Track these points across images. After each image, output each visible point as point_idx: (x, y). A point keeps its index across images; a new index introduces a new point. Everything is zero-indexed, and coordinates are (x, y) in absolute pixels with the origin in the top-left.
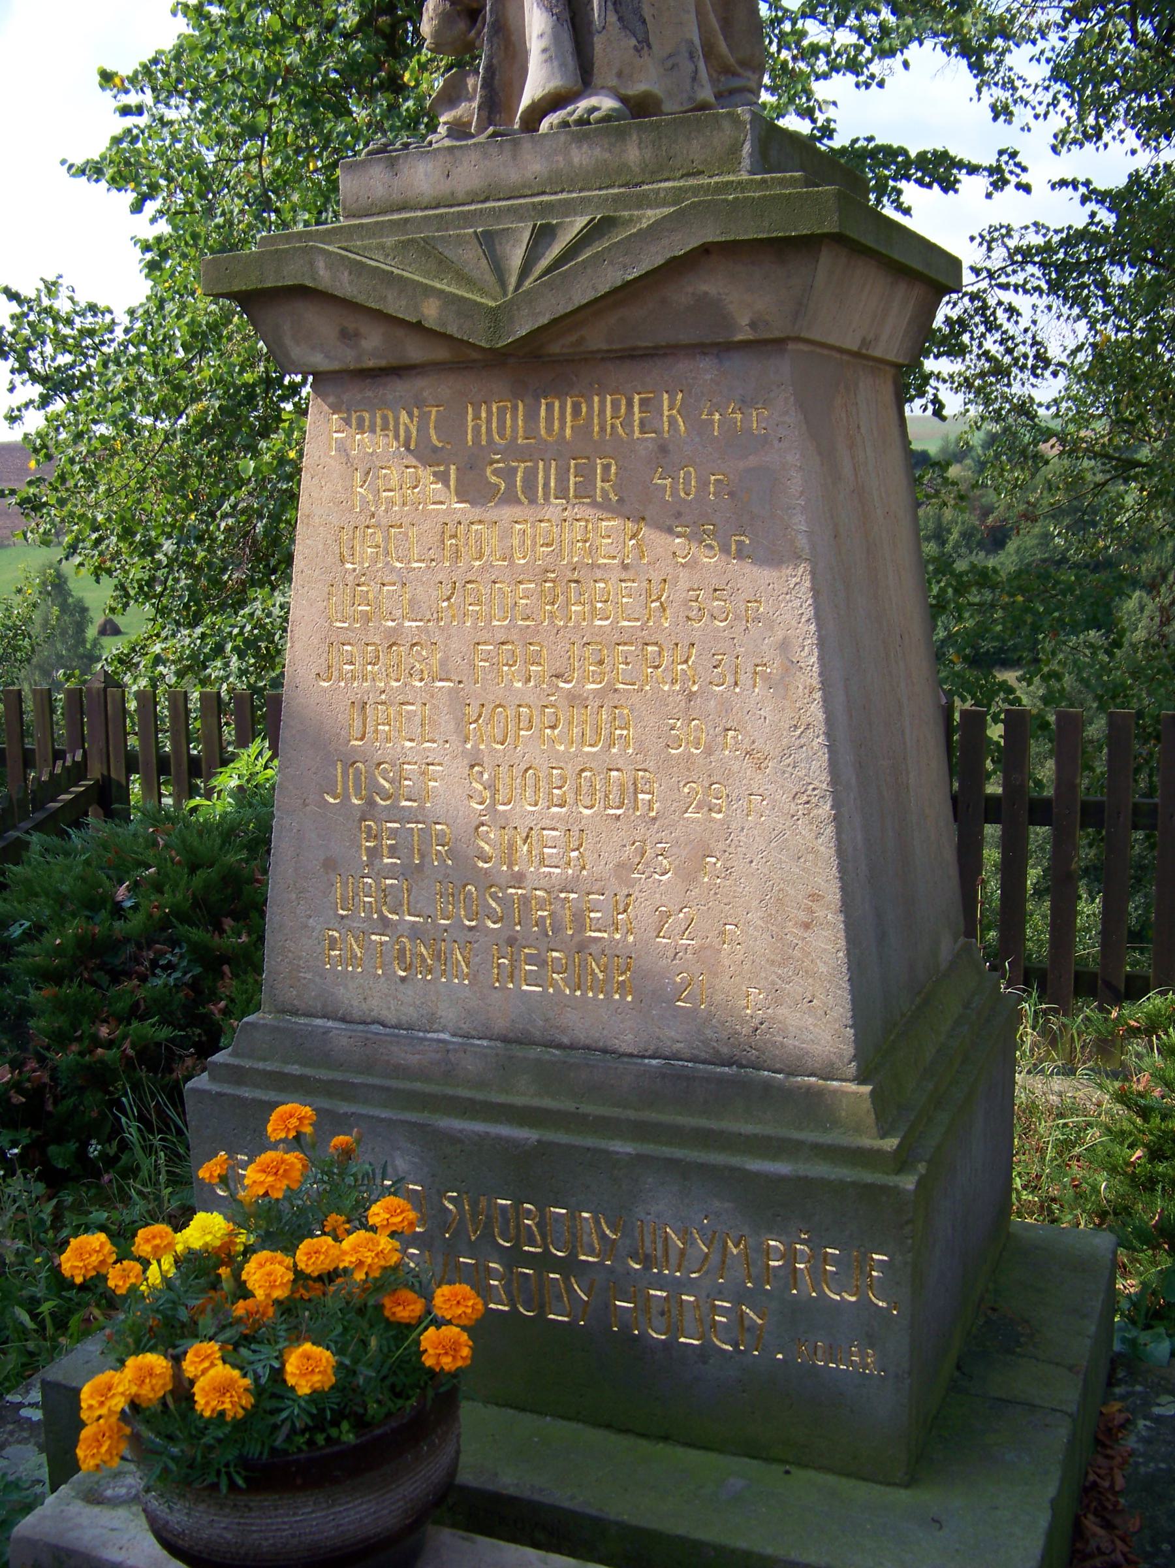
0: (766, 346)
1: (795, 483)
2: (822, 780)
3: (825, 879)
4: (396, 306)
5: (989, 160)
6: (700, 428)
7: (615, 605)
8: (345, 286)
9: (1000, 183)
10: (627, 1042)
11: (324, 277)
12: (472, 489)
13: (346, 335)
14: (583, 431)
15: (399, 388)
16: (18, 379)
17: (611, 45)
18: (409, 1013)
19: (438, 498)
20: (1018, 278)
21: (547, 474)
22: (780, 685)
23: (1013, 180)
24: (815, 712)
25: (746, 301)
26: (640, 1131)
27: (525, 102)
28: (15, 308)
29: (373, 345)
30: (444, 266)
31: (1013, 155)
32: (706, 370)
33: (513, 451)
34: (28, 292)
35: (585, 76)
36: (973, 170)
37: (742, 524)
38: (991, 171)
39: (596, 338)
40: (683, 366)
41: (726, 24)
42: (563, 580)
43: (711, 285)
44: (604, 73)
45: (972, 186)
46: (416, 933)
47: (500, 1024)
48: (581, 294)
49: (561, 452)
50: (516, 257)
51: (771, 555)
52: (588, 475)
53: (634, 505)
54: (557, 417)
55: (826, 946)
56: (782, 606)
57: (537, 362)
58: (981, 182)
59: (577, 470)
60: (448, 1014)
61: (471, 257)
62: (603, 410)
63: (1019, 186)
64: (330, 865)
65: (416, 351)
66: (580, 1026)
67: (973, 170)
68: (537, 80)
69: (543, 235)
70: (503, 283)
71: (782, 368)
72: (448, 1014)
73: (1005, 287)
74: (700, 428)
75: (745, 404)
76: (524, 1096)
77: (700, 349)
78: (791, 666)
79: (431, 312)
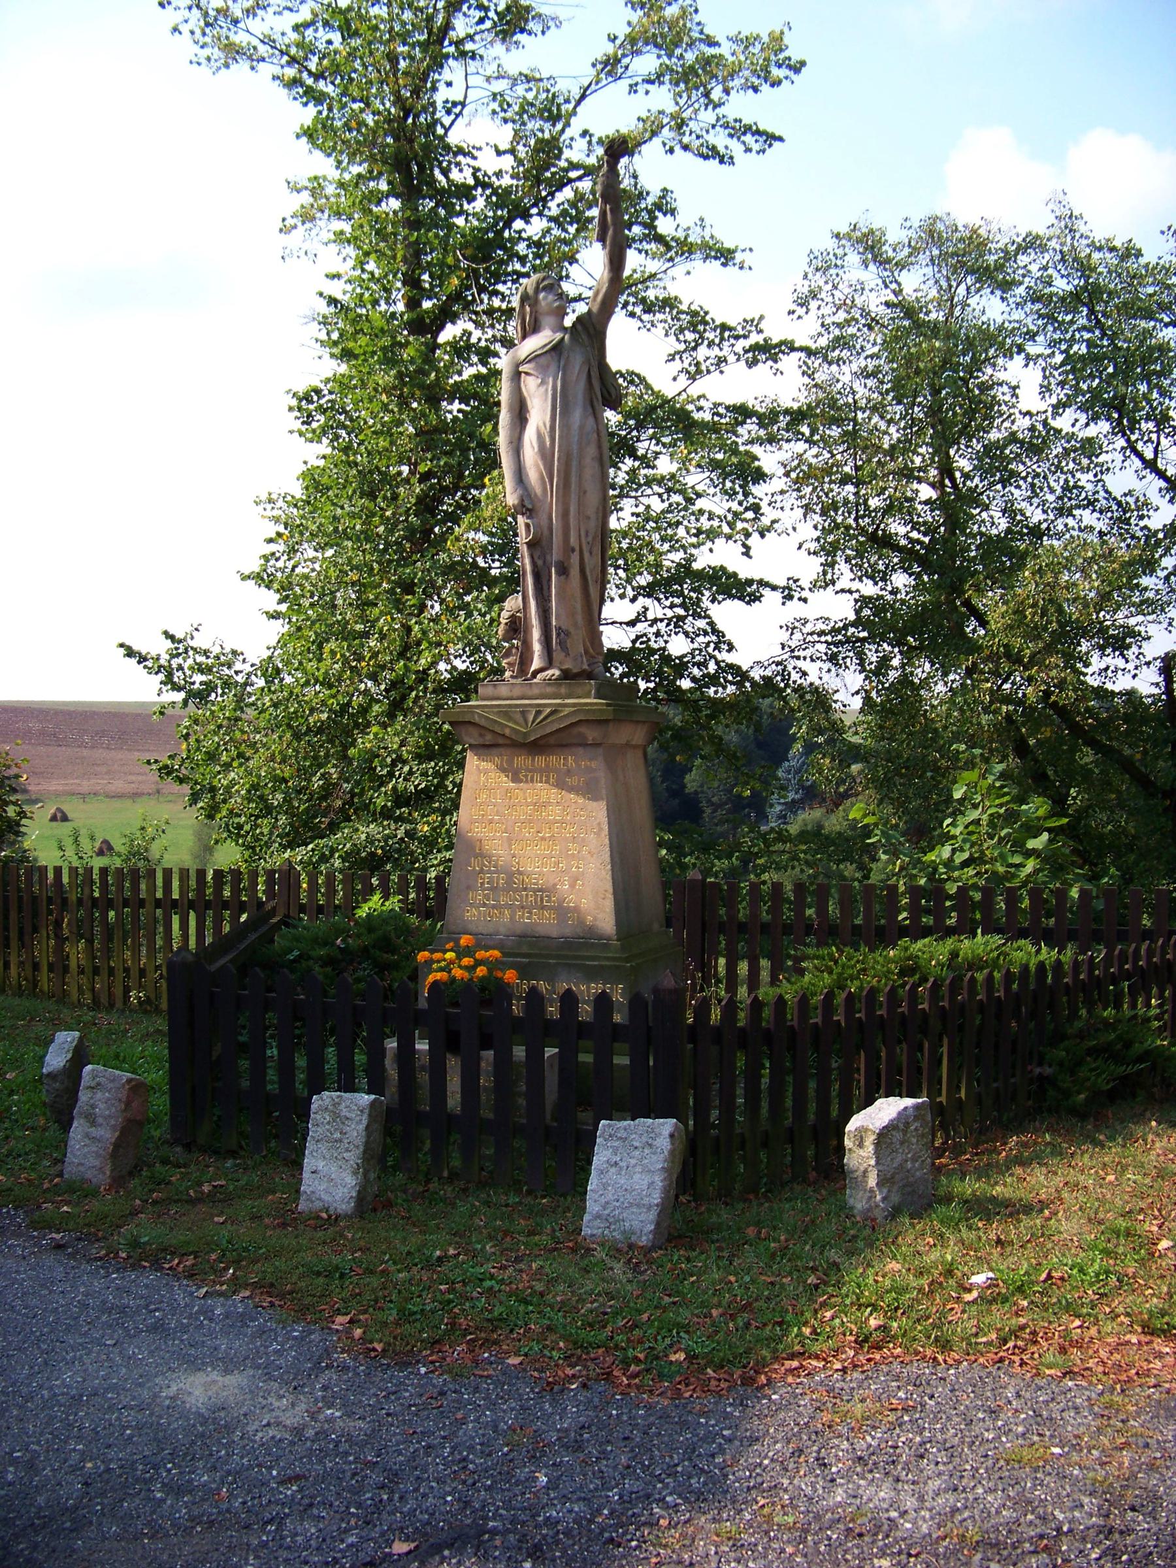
0: (596, 745)
1: (603, 781)
2: (608, 859)
3: (609, 886)
4: (498, 729)
5: (783, 583)
6: (579, 766)
7: (554, 813)
8: (483, 722)
9: (790, 597)
10: (554, 934)
11: (477, 719)
12: (516, 779)
13: (481, 735)
14: (547, 766)
15: (495, 751)
16: (164, 688)
17: (558, 655)
18: (491, 930)
19: (505, 781)
20: (808, 653)
21: (537, 776)
22: (598, 834)
23: (797, 595)
24: (607, 841)
25: (591, 734)
26: (558, 957)
27: (533, 668)
28: (169, 644)
29: (489, 738)
30: (510, 719)
31: (796, 581)
32: (581, 750)
33: (528, 770)
34: (179, 635)
35: (550, 663)
36: (774, 588)
37: (589, 791)
38: (784, 588)
39: (552, 740)
40: (574, 749)
41: (592, 644)
42: (540, 806)
43: (583, 729)
44: (556, 663)
45: (771, 598)
46: (494, 907)
47: (518, 932)
48: (548, 731)
49: (541, 771)
50: (531, 718)
51: (595, 798)
52: (548, 777)
53: (561, 785)
54: (540, 761)
55: (609, 904)
56: (598, 812)
57: (537, 747)
58: (777, 596)
59: (545, 774)
60: (502, 930)
61: (518, 717)
62: (553, 759)
63: (800, 599)
64: (469, 888)
65: (501, 741)
66: (541, 931)
67: (774, 588)
68: (536, 664)
69: (538, 713)
70: (526, 721)
71: (600, 750)
72: (502, 930)
73: (798, 658)
74: (579, 766)
75: (591, 760)
76: (525, 950)
77: (580, 745)
78: (601, 829)
79: (507, 732)
